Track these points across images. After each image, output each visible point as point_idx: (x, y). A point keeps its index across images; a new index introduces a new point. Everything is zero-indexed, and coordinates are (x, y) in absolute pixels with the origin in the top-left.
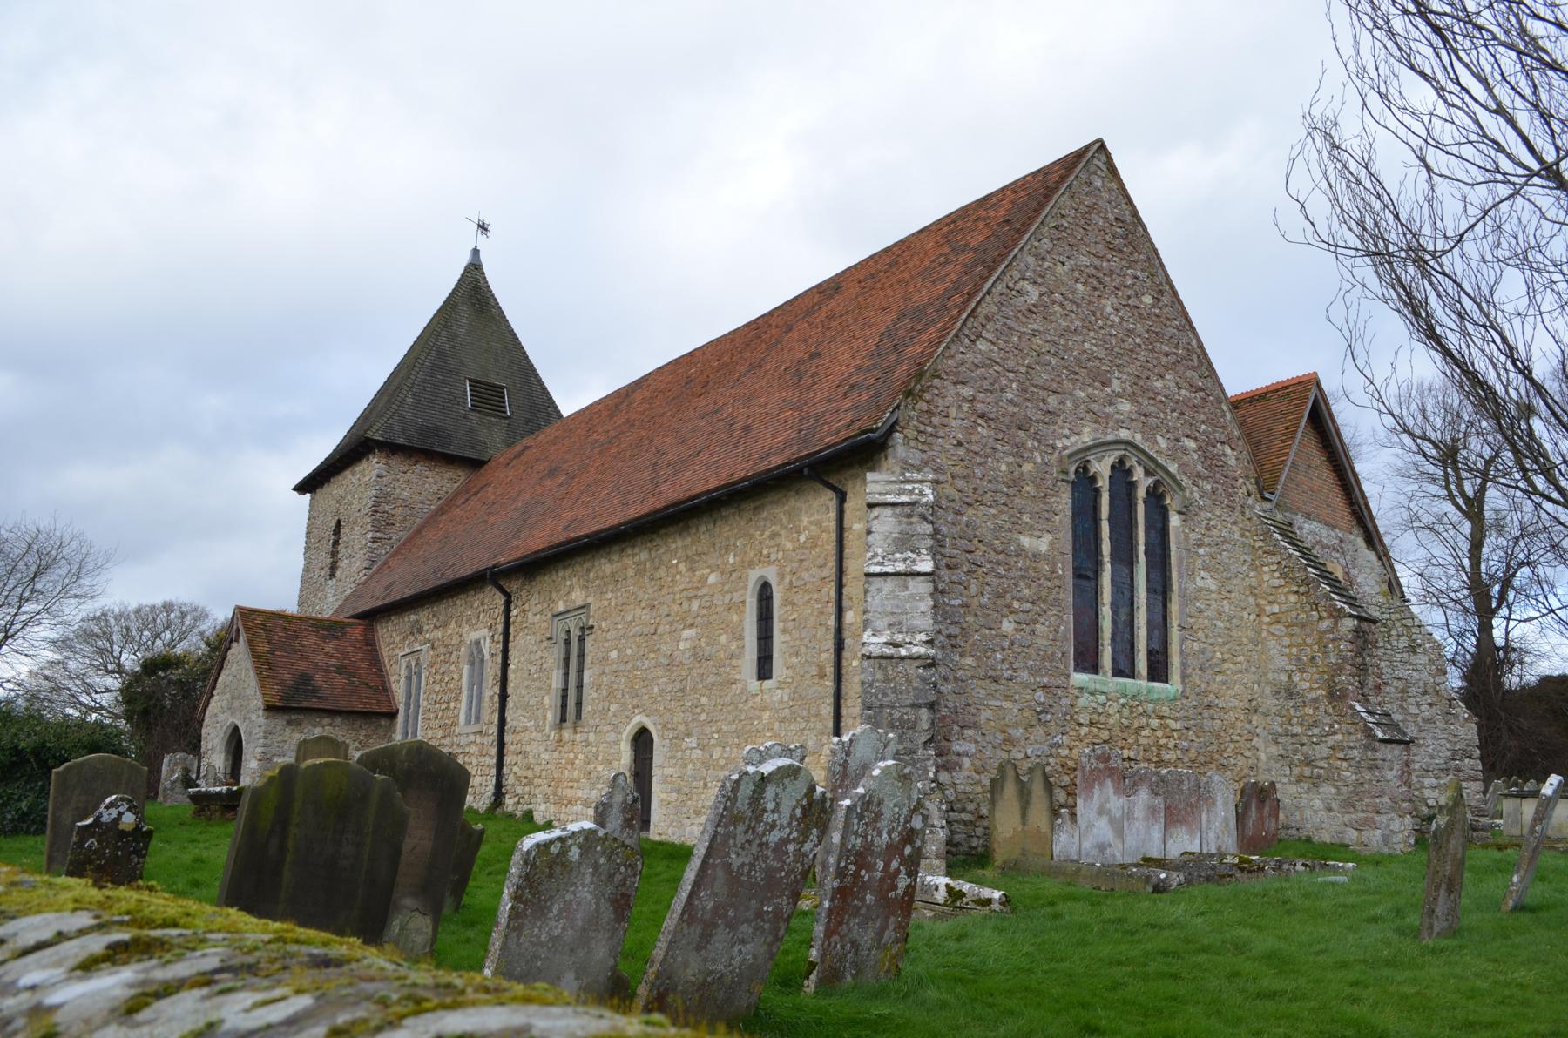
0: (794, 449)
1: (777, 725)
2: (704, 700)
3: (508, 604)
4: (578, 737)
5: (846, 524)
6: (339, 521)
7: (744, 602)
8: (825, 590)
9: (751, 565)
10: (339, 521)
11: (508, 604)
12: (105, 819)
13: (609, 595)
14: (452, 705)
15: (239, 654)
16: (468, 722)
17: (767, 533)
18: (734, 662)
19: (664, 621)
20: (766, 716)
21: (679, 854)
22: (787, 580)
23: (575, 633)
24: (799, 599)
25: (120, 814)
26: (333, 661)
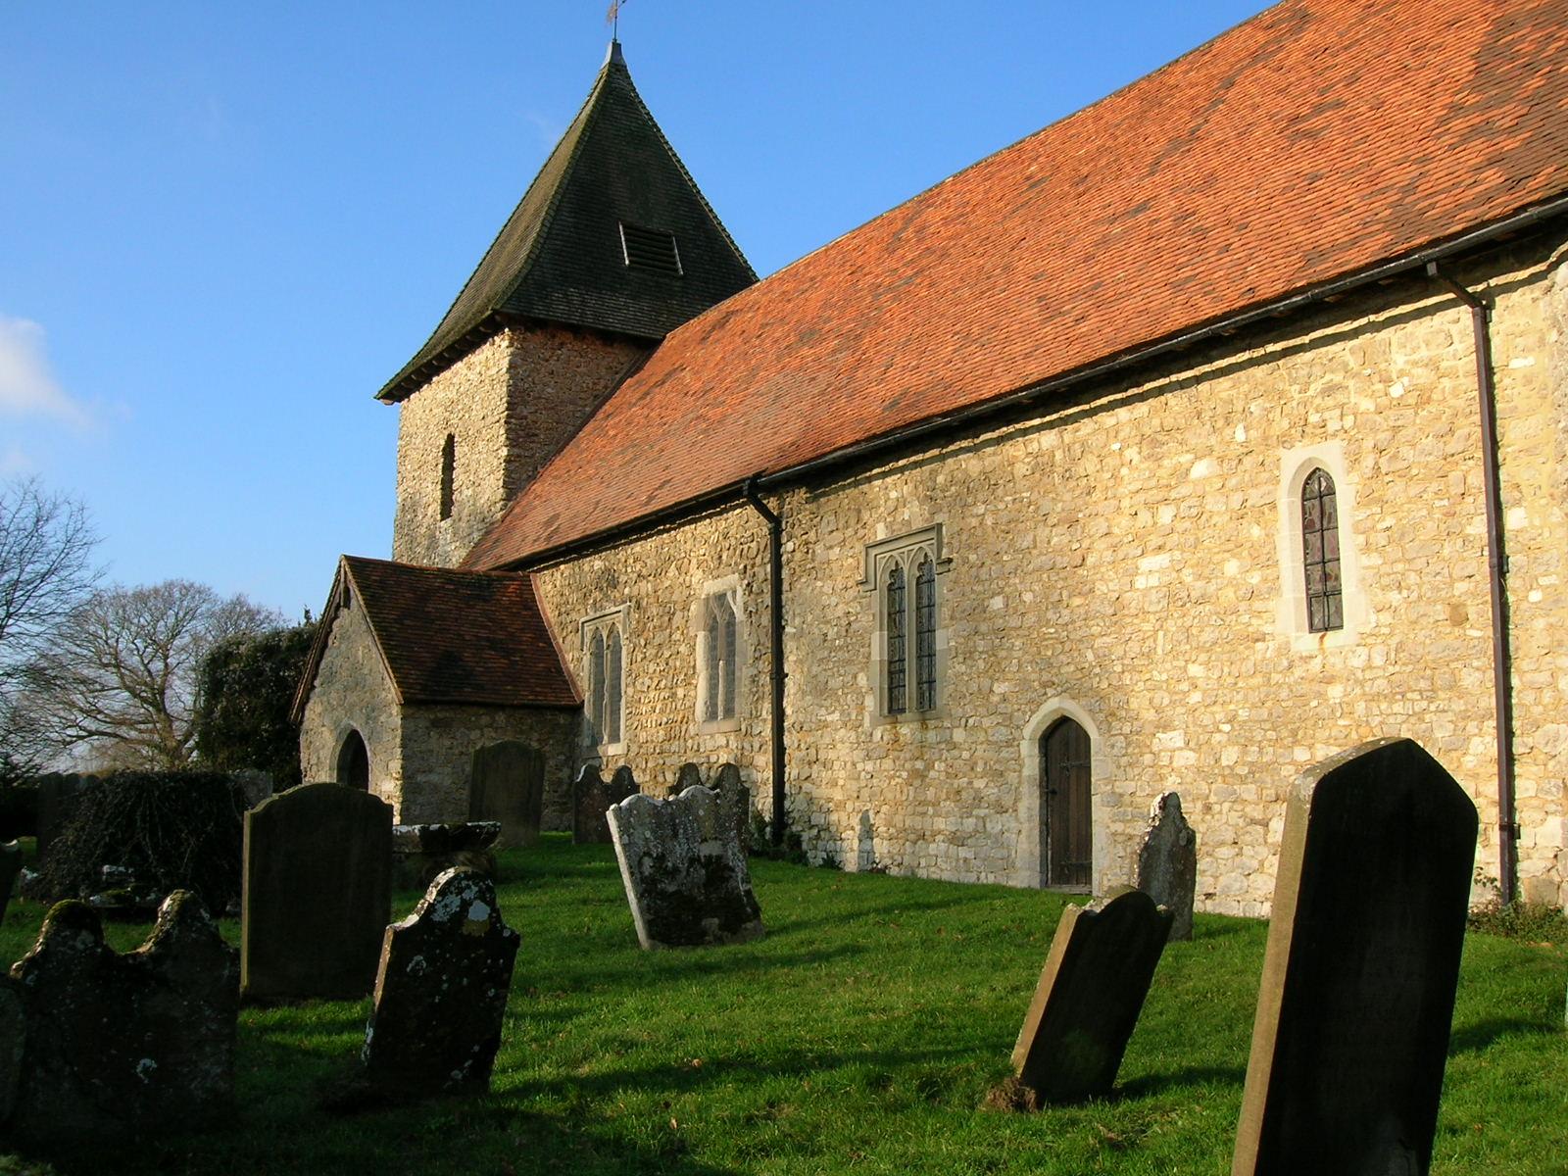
0: (1384, 238)
1: (1360, 707)
2: (1194, 670)
3: (776, 533)
4: (931, 736)
5: (1496, 359)
6: (451, 438)
7: (1273, 506)
8: (1455, 476)
9: (1284, 441)
10: (451, 438)
11: (776, 533)
12: (439, 916)
13: (981, 509)
14: (680, 692)
15: (354, 618)
16: (712, 715)
17: (1315, 387)
18: (1258, 605)
19: (1100, 545)
20: (1335, 692)
21: (1248, 930)
22: (1368, 461)
23: (909, 573)
24: (1396, 491)
25: (465, 905)
26: (483, 633)
